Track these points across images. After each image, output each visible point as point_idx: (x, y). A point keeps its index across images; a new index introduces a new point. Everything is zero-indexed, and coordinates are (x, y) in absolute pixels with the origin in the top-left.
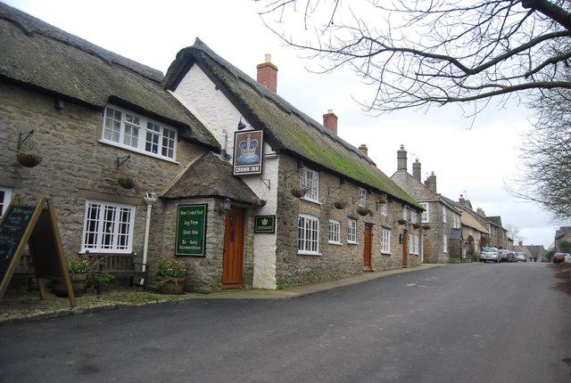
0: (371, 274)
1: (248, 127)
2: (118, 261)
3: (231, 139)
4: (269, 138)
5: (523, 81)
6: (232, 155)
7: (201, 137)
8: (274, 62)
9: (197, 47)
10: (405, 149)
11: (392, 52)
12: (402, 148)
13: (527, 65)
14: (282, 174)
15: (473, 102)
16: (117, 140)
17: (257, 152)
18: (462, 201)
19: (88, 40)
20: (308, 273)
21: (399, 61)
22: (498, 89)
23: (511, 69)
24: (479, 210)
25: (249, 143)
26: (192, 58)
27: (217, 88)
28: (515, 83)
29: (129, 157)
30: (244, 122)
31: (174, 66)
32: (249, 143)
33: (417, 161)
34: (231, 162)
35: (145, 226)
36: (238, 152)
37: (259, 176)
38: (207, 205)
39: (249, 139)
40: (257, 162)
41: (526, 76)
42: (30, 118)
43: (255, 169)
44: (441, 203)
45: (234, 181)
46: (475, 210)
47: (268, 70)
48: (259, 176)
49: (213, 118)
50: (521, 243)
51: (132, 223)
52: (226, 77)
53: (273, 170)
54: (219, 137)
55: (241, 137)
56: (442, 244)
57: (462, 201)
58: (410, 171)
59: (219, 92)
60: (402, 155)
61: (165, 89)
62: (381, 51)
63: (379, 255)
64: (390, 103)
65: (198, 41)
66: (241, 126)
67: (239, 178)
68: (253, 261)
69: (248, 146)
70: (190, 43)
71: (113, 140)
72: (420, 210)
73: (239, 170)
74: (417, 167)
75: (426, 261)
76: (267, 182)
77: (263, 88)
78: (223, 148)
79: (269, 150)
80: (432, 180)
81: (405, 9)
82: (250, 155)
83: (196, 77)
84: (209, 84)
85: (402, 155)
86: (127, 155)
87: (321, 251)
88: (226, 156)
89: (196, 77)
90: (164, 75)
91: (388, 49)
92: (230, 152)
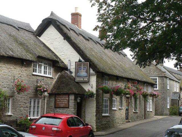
0: (129, 123)
1: (83, 61)
2: (14, 123)
4: (93, 66)
7: (61, 65)
8: (79, 11)
9: (51, 17)
14: (97, 82)
16: (41, 73)
17: (87, 72)
19: (5, 16)
20: (106, 124)
25: (82, 68)
29: (43, 79)
30: (81, 59)
34: (73, 75)
35: (44, 106)
36: (77, 71)
37: (87, 82)
39: (82, 66)
42: (16, 70)
43: (86, 79)
44: (166, 77)
45: (77, 85)
47: (76, 17)
48: (87, 82)
49: (63, 53)
51: (40, 105)
52: (65, 30)
53: (93, 80)
54: (66, 62)
55: (78, 64)
56: (167, 103)
59: (66, 41)
61: (36, 36)
63: (132, 113)
65: (52, 14)
67: (77, 83)
68: (85, 120)
69: (82, 69)
71: (39, 73)
72: (153, 85)
73: (77, 79)
75: (156, 114)
77: (75, 27)
78: (69, 68)
79: (92, 71)
82: (83, 73)
83: (51, 33)
84: (59, 37)
86: (42, 78)
87: (109, 114)
88: (71, 72)
89: (51, 33)
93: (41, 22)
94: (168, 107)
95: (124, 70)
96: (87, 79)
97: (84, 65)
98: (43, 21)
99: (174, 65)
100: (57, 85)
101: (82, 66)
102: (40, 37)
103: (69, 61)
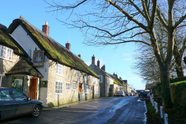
1: (38, 49)
3: (32, 53)
5: (130, 39)
6: (33, 59)
9: (20, 19)
10: (94, 56)
11: (72, 9)
12: (93, 56)
13: (131, 34)
15: (114, 45)
17: (42, 58)
18: (114, 74)
21: (91, 30)
22: (122, 41)
23: (128, 35)
24: (120, 78)
25: (39, 55)
26: (18, 23)
27: (28, 34)
28: (128, 40)
31: (11, 25)
32: (39, 55)
33: (98, 60)
34: (32, 61)
38: (23, 77)
39: (39, 54)
40: (42, 62)
41: (131, 38)
46: (119, 78)
49: (26, 45)
50: (134, 89)
55: (36, 52)
57: (114, 74)
58: (96, 64)
59: (28, 36)
60: (93, 58)
62: (85, 26)
64: (90, 43)
66: (36, 49)
70: (18, 18)
74: (98, 62)
76: (45, 69)
77: (43, 34)
78: (29, 56)
80: (104, 67)
81: (88, 14)
82: (39, 59)
85: (93, 58)
88: (31, 59)
89: (20, 29)
90: (8, 27)
91: (88, 26)
92: (32, 58)
93: (12, 22)
94: (29, 85)
95: (87, 81)
96: (42, 64)
97: (40, 53)
98: (14, 21)
99: (99, 61)
100: (177, 97)
101: (39, 54)
102: (11, 34)
103: (30, 50)
